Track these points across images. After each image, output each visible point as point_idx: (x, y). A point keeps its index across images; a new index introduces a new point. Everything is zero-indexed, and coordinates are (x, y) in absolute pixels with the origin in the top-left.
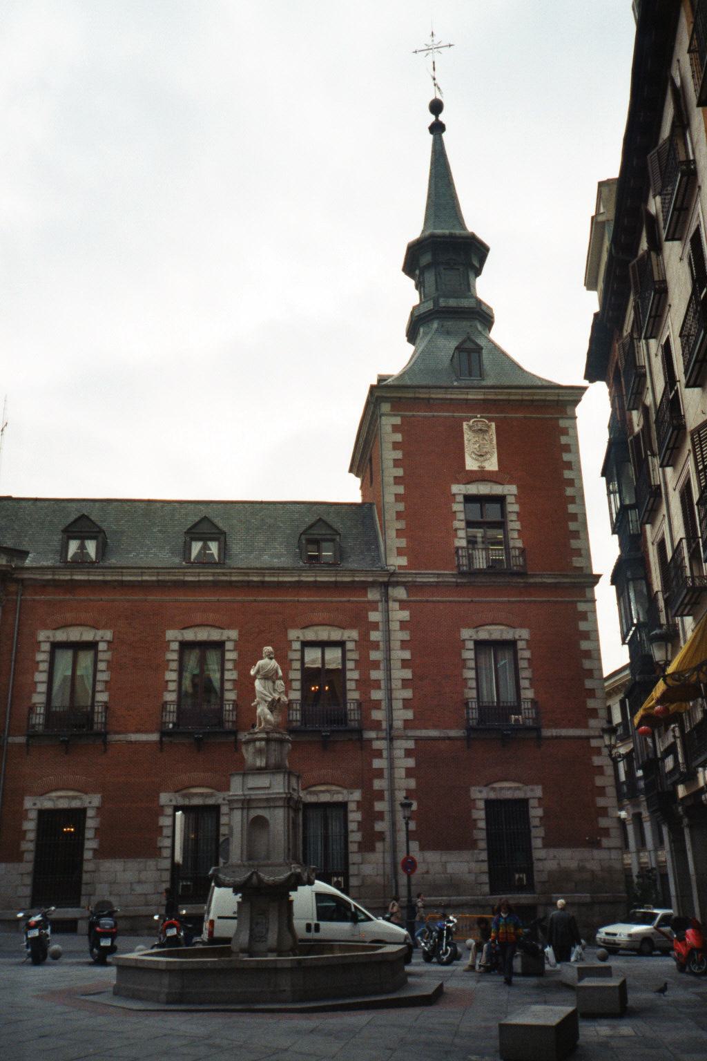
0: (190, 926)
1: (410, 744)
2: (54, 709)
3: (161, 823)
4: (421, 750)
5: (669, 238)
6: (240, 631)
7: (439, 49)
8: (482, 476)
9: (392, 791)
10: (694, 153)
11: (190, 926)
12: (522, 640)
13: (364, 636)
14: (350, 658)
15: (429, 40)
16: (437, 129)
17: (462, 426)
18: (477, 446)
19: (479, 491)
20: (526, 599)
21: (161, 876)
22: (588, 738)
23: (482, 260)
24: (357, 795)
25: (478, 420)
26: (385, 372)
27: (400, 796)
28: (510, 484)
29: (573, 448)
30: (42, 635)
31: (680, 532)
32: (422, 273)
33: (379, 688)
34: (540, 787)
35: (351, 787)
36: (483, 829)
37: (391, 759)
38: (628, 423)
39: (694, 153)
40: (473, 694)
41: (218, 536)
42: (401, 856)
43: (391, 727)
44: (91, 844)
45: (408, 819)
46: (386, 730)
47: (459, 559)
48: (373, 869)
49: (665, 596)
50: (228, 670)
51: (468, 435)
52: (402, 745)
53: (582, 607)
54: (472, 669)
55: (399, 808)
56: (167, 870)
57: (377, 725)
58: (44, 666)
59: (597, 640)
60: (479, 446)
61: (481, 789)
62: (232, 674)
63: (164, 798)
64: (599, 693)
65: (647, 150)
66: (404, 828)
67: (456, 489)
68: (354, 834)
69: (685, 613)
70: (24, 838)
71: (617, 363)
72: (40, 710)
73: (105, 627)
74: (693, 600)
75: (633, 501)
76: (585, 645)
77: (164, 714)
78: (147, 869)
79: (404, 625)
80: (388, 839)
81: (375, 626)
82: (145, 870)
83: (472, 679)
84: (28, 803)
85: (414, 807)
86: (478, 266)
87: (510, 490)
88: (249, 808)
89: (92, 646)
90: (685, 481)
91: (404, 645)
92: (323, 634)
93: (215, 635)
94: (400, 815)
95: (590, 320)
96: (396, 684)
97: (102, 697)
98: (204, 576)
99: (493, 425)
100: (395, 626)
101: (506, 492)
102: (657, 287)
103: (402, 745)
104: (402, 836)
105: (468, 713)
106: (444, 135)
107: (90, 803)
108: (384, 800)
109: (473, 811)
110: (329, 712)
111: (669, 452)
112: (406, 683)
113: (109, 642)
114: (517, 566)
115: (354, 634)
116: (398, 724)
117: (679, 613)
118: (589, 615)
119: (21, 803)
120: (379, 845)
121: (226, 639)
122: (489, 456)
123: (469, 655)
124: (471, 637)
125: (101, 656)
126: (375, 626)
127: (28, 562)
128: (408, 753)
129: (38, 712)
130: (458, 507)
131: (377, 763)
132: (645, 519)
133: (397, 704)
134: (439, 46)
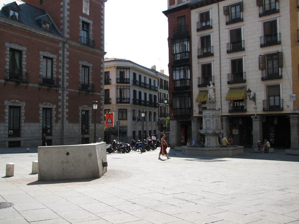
1: (67, 93)
4: (70, 95)
20: (90, 55)
21: (6, 128)
22: (100, 96)
37: (63, 97)
41: (19, 11)
44: (23, 118)
56: (7, 126)
88: (206, 118)
98: (19, 25)
103: (66, 93)
116: (65, 86)
120: (59, 121)
128: (67, 95)
131: (60, 97)
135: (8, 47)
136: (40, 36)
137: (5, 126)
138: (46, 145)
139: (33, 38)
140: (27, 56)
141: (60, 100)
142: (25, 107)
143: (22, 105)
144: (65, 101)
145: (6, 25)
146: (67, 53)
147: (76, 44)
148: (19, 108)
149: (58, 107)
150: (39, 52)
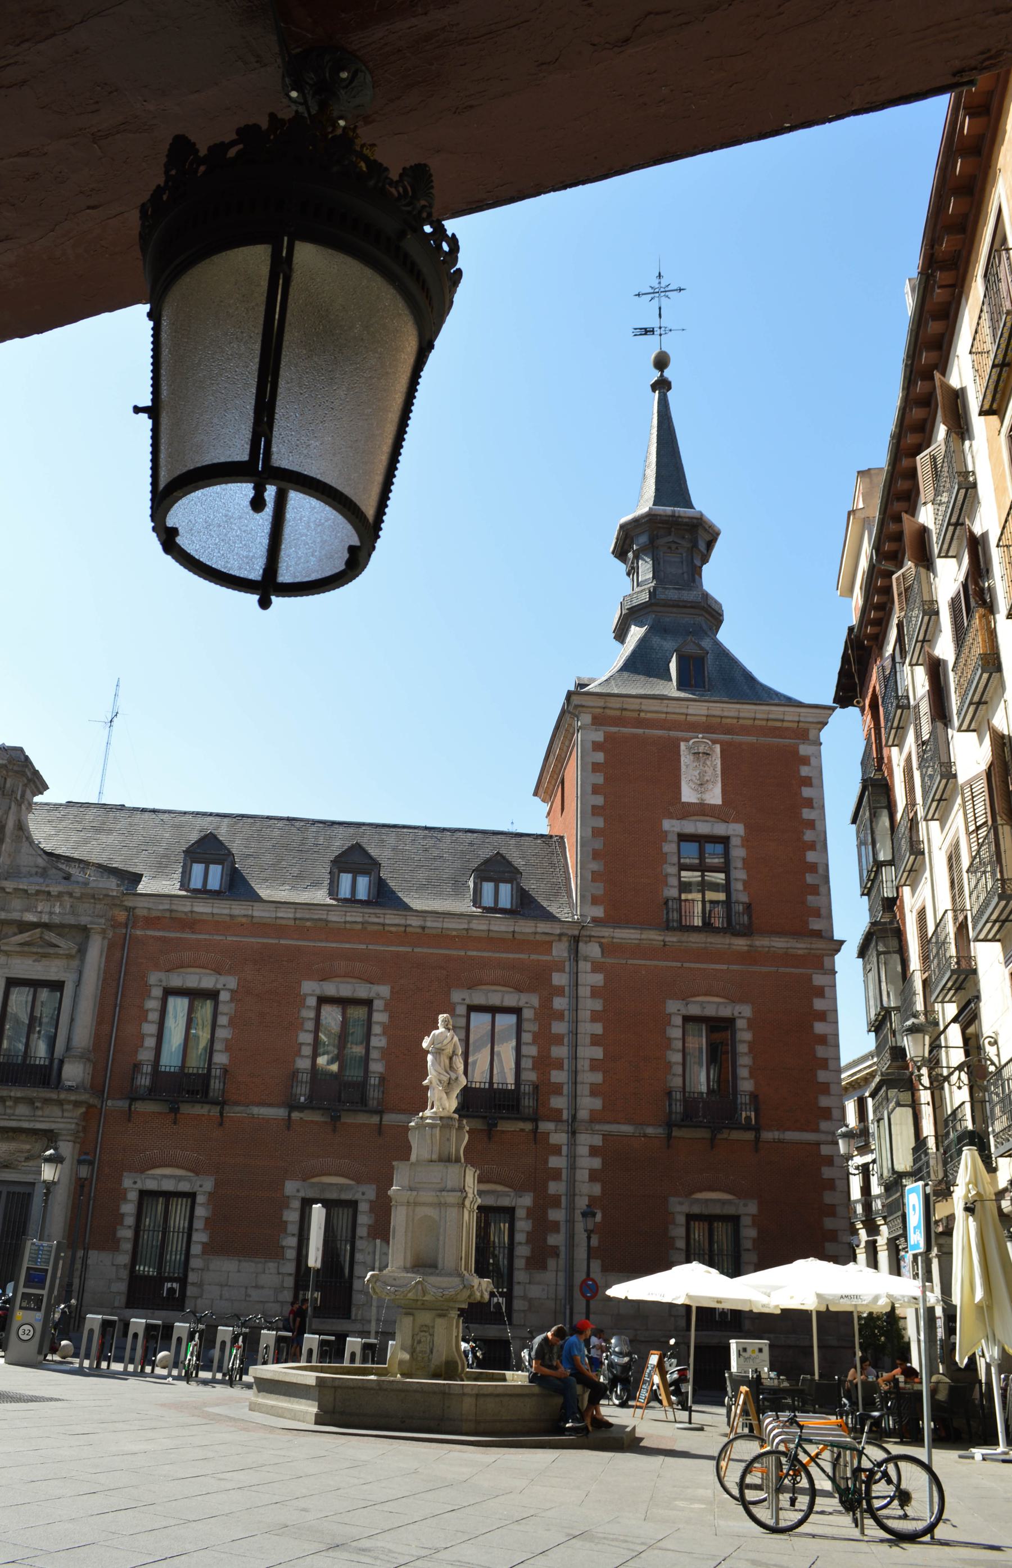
0: (165, 197)
1: (597, 1141)
2: (163, 1069)
3: (285, 1218)
5: (942, 555)
6: (392, 988)
7: (667, 293)
8: (702, 810)
9: (572, 1195)
10: (974, 463)
11: (165, 197)
12: (743, 1017)
13: (546, 1004)
14: (527, 1029)
15: (655, 283)
16: (662, 386)
17: (679, 746)
18: (696, 773)
19: (696, 830)
22: (818, 1144)
23: (710, 545)
24: (526, 1200)
25: (700, 740)
26: (585, 675)
27: (582, 1203)
28: (736, 822)
29: (815, 781)
30: (153, 978)
31: (945, 902)
32: (637, 557)
33: (561, 1094)
34: (756, 1201)
35: (520, 1189)
36: (682, 1250)
37: (572, 1158)
38: (886, 761)
39: (974, 463)
40: (678, 1082)
42: (580, 1276)
43: (574, 1117)
45: (589, 1233)
46: (568, 1121)
47: (667, 913)
48: (543, 1290)
49: (924, 978)
50: (376, 1035)
51: (686, 759)
52: (586, 1140)
53: (818, 980)
54: (678, 1051)
55: (578, 1217)
56: (290, 1274)
57: (555, 1116)
58: (153, 1016)
59: (836, 1022)
60: (699, 774)
61: (681, 1199)
62: (380, 1040)
63: (291, 1187)
64: (833, 1089)
65: (919, 449)
66: (586, 1244)
67: (667, 825)
68: (520, 1247)
69: (947, 999)
70: (121, 1223)
71: (874, 687)
72: (147, 1069)
73: (229, 973)
74: (957, 985)
75: (889, 857)
76: (819, 1028)
77: (295, 1084)
78: (267, 1272)
79: (595, 992)
80: (562, 1255)
81: (560, 991)
82: (264, 1272)
83: (678, 1063)
84: (127, 1183)
85: (599, 1217)
86: (705, 552)
87: (736, 830)
89: (213, 995)
90: (952, 841)
91: (595, 1017)
92: (495, 999)
93: (362, 991)
94: (580, 1227)
95: (841, 638)
96: (584, 1065)
97: (221, 1058)
99: (718, 748)
100: (584, 992)
101: (730, 832)
102: (926, 607)
103: (586, 1140)
104: (581, 1253)
105: (670, 1105)
106: (669, 394)
107: (201, 1186)
108: (563, 1070)
109: (671, 1227)
110: (497, 1096)
111: (935, 804)
112: (595, 1065)
113: (232, 991)
114: (739, 924)
115: (534, 1000)
116: (583, 1114)
117: (940, 999)
118: (827, 991)
119: (120, 1182)
120: (551, 1263)
121: (374, 995)
122: (710, 786)
123: (676, 1033)
124: (679, 1010)
125: (222, 1008)
126: (560, 991)
127: (141, 888)
128: (594, 1151)
129: (144, 1071)
130: (670, 847)
131: (555, 1162)
132: (903, 881)
133: (583, 1090)
134: (667, 289)
135: (311, 995)
136: (454, 936)
137: (279, 1273)
138: (917, 1387)
139: (416, 950)
140: (390, 1017)
141: (556, 1175)
142: (371, 1202)
143: (358, 1196)
144: (582, 1175)
145: (308, 924)
146: (593, 979)
147: (638, 936)
148: (353, 1204)
149: (544, 1203)
150: (448, 994)
